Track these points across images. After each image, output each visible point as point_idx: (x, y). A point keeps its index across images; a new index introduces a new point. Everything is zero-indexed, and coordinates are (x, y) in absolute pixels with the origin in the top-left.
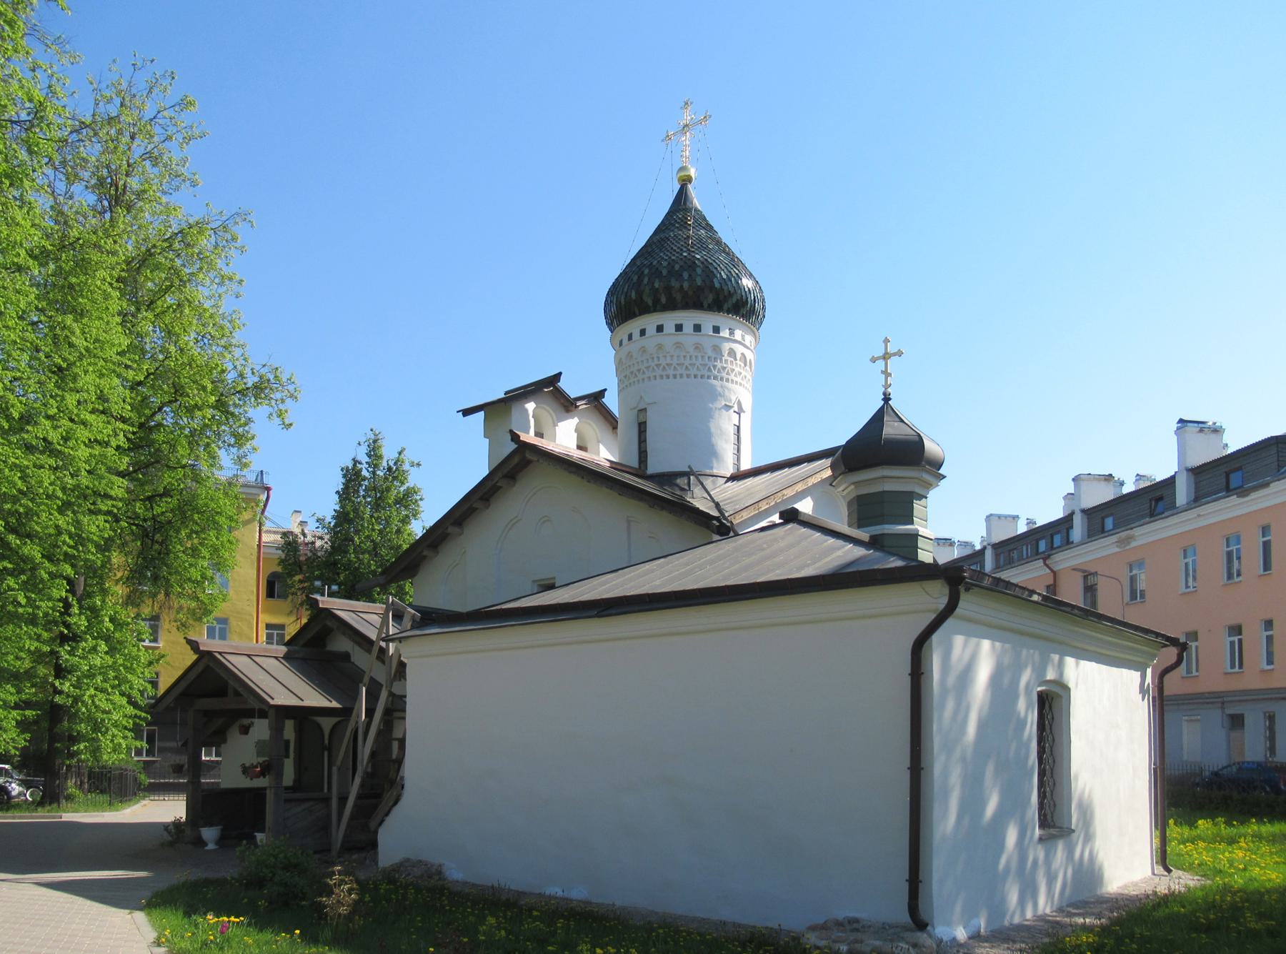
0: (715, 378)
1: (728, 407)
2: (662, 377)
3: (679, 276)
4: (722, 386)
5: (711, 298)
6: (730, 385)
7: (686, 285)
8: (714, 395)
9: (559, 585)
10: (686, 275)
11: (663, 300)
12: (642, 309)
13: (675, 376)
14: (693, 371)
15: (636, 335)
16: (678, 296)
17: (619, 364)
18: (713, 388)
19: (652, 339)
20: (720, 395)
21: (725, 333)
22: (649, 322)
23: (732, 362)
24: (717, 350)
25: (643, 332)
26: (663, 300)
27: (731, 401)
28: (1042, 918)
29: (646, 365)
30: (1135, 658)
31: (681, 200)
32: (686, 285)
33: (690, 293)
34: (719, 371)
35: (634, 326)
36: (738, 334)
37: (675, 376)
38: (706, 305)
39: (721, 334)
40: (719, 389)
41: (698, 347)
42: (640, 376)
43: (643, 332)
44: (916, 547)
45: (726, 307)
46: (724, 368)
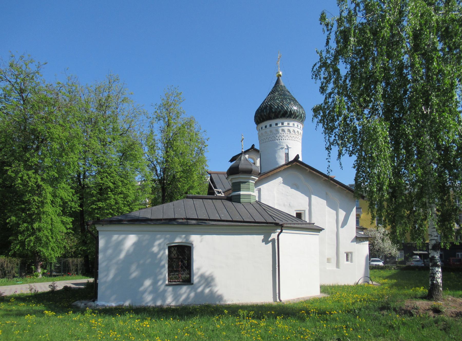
0: (277, 140)
1: (282, 148)
2: (271, 141)
3: (263, 111)
4: (279, 142)
5: (273, 115)
6: (282, 141)
7: (265, 114)
8: (277, 145)
9: (206, 204)
10: (265, 111)
11: (261, 119)
12: (264, 120)
13: (269, 141)
14: (270, 139)
15: (264, 128)
16: (264, 117)
17: (259, 137)
18: (276, 143)
19: (269, 128)
20: (279, 145)
21: (280, 125)
22: (267, 123)
23: (283, 133)
24: (277, 131)
25: (266, 127)
26: (261, 119)
27: (283, 146)
28: (73, 222)
29: (269, 136)
30: (263, 231)
31: (278, 82)
32: (265, 114)
33: (267, 116)
34: (278, 137)
35: (263, 125)
36: (286, 124)
37: (269, 141)
38: (272, 118)
39: (278, 125)
40: (278, 143)
41: (271, 131)
42: (265, 141)
43: (266, 127)
44: (240, 198)
45: (279, 116)
46: (280, 136)
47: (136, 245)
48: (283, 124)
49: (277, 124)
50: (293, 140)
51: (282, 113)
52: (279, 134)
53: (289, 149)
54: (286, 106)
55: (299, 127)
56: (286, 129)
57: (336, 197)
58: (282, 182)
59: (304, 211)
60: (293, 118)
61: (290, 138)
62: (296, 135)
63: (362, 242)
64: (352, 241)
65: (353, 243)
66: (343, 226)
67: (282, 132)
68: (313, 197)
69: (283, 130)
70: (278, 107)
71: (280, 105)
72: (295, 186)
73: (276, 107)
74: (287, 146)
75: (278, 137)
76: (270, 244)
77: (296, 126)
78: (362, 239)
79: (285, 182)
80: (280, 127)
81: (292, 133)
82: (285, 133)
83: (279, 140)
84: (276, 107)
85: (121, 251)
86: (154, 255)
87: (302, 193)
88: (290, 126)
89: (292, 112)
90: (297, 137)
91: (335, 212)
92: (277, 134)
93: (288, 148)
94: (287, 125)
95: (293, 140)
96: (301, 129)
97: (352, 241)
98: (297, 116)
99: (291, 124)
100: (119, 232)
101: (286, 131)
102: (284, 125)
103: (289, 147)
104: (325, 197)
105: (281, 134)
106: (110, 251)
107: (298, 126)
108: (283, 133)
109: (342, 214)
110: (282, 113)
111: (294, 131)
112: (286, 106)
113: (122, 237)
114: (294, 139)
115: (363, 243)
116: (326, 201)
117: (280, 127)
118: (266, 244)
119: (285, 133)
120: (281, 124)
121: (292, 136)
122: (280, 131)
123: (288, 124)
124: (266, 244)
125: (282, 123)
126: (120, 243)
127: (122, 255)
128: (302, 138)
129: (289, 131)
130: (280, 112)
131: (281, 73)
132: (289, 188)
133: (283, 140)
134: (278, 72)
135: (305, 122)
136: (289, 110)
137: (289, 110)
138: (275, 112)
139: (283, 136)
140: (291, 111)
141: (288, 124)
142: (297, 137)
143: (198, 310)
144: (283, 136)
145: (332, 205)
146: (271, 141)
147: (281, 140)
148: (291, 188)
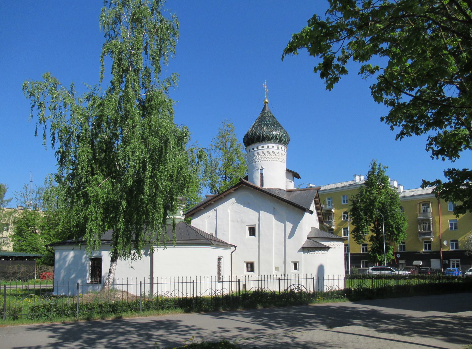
1: (258, 169)
2: (262, 161)
4: (255, 164)
21: (256, 149)
36: (260, 147)
39: (254, 150)
40: (255, 165)
45: (255, 141)
46: (256, 159)
47: (75, 257)
48: (257, 148)
49: (253, 149)
51: (255, 139)
54: (259, 132)
55: (283, 149)
56: (260, 152)
57: (282, 210)
58: (235, 201)
59: (255, 225)
60: (268, 141)
62: (271, 155)
63: (311, 251)
64: (299, 251)
65: (299, 253)
66: (290, 237)
67: (257, 155)
68: (261, 212)
69: (258, 153)
70: (252, 134)
71: (254, 132)
72: (247, 204)
73: (251, 134)
74: (262, 167)
76: (149, 257)
78: (310, 249)
79: (238, 202)
80: (256, 150)
84: (251, 134)
85: (66, 262)
86: (83, 264)
87: (253, 209)
89: (265, 136)
91: (283, 224)
93: (263, 169)
94: (261, 148)
97: (299, 251)
98: (271, 139)
99: (265, 146)
100: (66, 250)
101: (261, 154)
104: (274, 212)
106: (61, 262)
107: (278, 148)
109: (289, 226)
110: (255, 139)
111: (278, 153)
112: (259, 132)
113: (67, 253)
114: (269, 159)
115: (312, 253)
116: (273, 216)
118: (146, 256)
121: (266, 157)
122: (256, 154)
123: (263, 147)
124: (146, 256)
126: (67, 256)
127: (67, 265)
129: (263, 153)
130: (254, 137)
131: (267, 101)
132: (242, 206)
134: (265, 100)
136: (261, 135)
137: (261, 135)
138: (251, 139)
139: (258, 158)
140: (263, 136)
141: (263, 147)
143: (228, 309)
144: (258, 158)
145: (280, 219)
146: (262, 161)
148: (244, 206)
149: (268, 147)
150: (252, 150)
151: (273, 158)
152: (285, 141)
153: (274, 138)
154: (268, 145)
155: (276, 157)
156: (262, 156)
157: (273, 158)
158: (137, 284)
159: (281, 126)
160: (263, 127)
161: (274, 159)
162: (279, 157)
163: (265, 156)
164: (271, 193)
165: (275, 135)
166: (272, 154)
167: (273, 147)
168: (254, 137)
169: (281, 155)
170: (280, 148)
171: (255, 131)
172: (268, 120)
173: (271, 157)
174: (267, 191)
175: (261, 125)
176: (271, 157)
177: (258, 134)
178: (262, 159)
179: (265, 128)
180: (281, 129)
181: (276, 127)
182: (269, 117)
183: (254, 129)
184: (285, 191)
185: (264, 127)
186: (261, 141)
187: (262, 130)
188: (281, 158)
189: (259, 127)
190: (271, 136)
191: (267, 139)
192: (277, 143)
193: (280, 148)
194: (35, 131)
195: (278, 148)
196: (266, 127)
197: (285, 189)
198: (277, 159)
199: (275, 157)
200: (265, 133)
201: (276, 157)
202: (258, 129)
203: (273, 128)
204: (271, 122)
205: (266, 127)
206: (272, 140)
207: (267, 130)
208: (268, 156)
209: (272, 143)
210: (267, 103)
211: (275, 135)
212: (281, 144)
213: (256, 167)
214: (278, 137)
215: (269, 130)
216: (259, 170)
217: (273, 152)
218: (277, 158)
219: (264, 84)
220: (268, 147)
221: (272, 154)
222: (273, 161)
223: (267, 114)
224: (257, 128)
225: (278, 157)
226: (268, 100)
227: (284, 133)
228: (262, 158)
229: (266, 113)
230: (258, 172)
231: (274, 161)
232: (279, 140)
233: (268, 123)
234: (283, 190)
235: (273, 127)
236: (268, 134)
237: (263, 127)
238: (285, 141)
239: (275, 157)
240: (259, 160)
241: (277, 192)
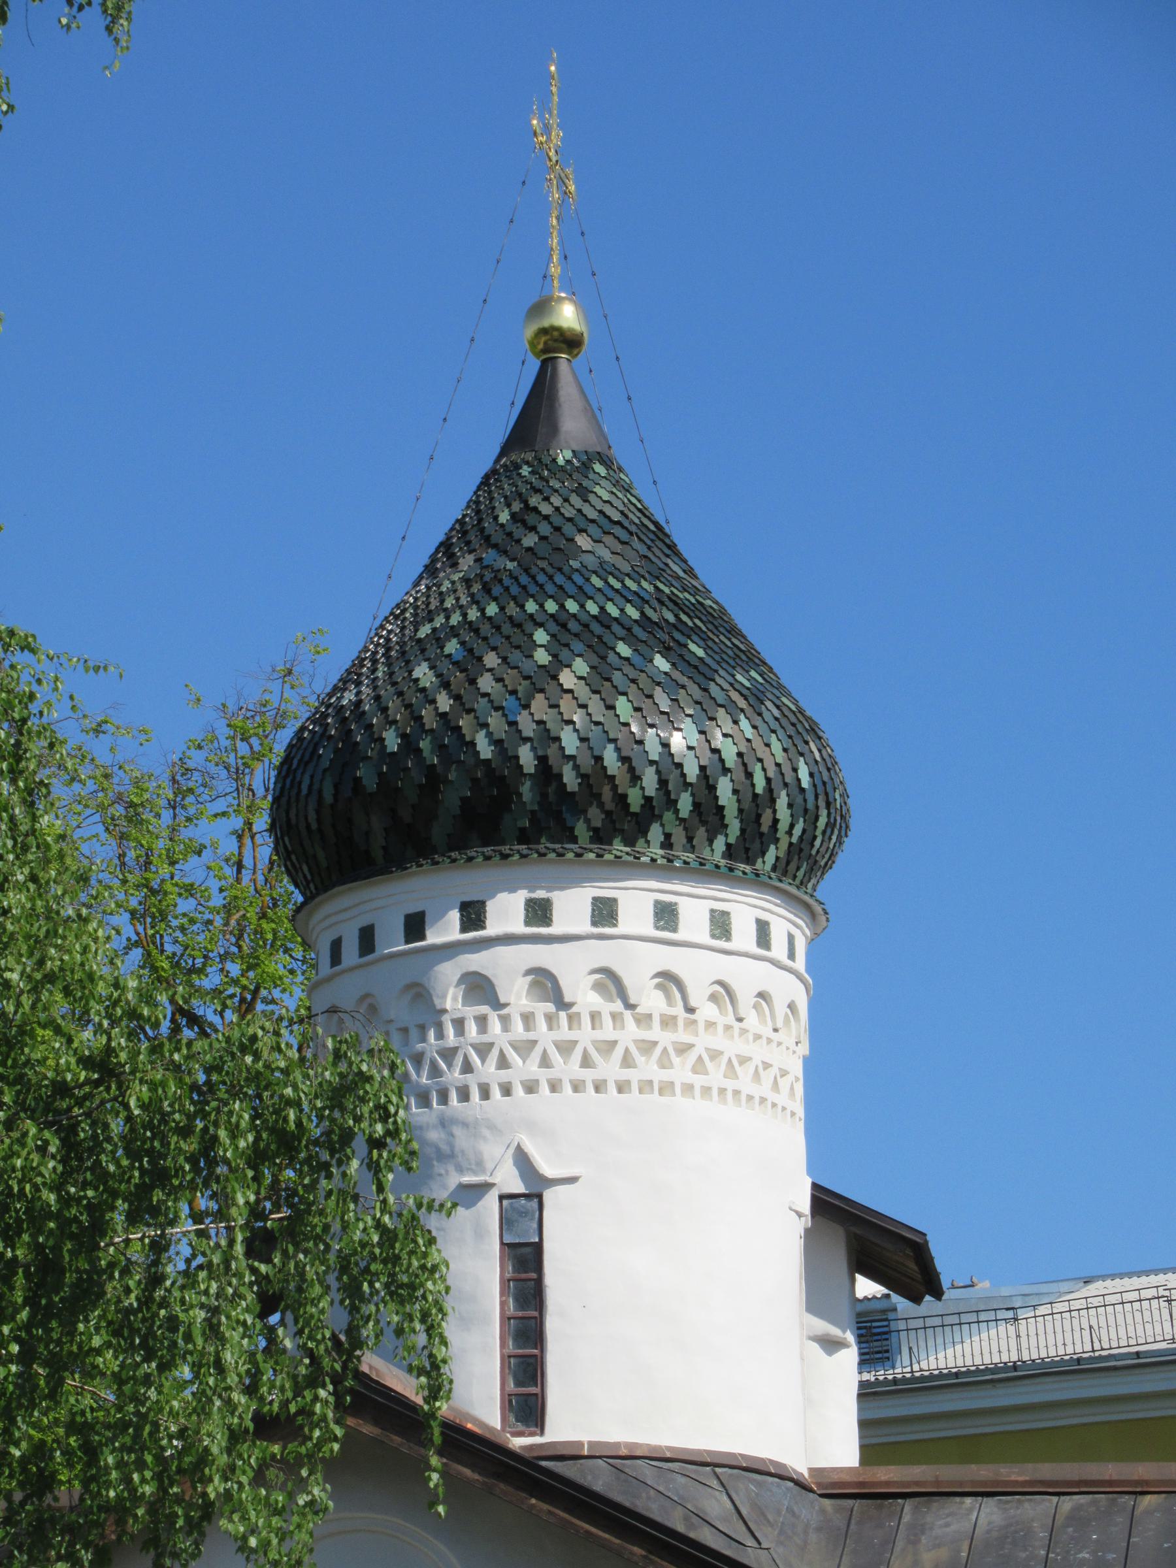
1: (474, 1192)
4: (444, 1123)
23: (482, 1021)
27: (480, 1166)
39: (434, 937)
40: (434, 1135)
45: (438, 833)
46: (448, 1054)
48: (473, 915)
49: (415, 926)
50: (646, 1086)
51: (451, 800)
52: (440, 1035)
53: (549, 1196)
54: (495, 721)
55: (779, 950)
60: (600, 837)
61: (568, 1068)
62: (644, 1020)
67: (471, 1012)
70: (409, 744)
71: (430, 721)
73: (392, 741)
74: (523, 1161)
75: (435, 1072)
77: (702, 934)
80: (451, 950)
81: (707, 1011)
82: (505, 1021)
83: (444, 1098)
84: (392, 741)
88: (554, 930)
89: (570, 779)
90: (665, 1038)
92: (423, 1029)
94: (705, 939)
95: (646, 1086)
96: (800, 964)
98: (650, 812)
102: (493, 928)
103: (548, 1169)
105: (459, 1024)
107: (721, 925)
108: (482, 1021)
110: (451, 800)
111: (725, 992)
112: (495, 721)
114: (609, 1069)
117: (451, 950)
119: (505, 1021)
120: (455, 916)
121: (585, 1035)
122: (452, 1000)
123: (539, 912)
125: (465, 907)
128: (807, 1061)
130: (433, 779)
131: (567, 315)
132: (941, 1277)
133: (485, 1094)
134: (542, 306)
135: (829, 886)
136: (526, 757)
139: (483, 1050)
140: (546, 773)
141: (539, 912)
142: (665, 1038)
147: (464, 1095)
149: (605, 912)
150: (393, 944)
151: (664, 1062)
152: (808, 838)
153: (685, 803)
154: (605, 890)
155: (703, 1041)
156: (528, 1019)
157: (664, 1062)
158: (925, 1328)
159: (749, 658)
160: (542, 657)
161: (681, 1072)
162: (732, 1047)
163: (564, 1032)
164: (654, 1510)
165: (692, 772)
166: (652, 1001)
167: (666, 915)
168: (433, 779)
169: (752, 1020)
170: (744, 935)
171: (444, 703)
172: (604, 570)
173: (647, 1047)
174: (599, 1480)
175: (523, 626)
176: (647, 1047)
177: (485, 750)
178: (524, 1068)
179: (567, 679)
180: (755, 697)
181: (700, 672)
182: (605, 526)
183: (423, 673)
184: (799, 1484)
185: (559, 663)
186: (524, 837)
187: (539, 704)
188: (758, 1052)
189: (491, 660)
190: (650, 780)
191: (596, 816)
192: (703, 872)
193: (744, 935)
194: (252, 856)
195: (721, 925)
196: (581, 666)
197: (800, 1466)
198: (715, 1076)
199: (683, 1049)
200: (570, 742)
201: (703, 1041)
202: (486, 683)
203: (671, 684)
204: (640, 600)
205: (581, 666)
206: (655, 833)
207: (596, 706)
208: (608, 1031)
209: (653, 868)
210: (571, 342)
211: (692, 772)
212: (756, 881)
213: (448, 1156)
214: (724, 790)
215: (623, 706)
216: (490, 1206)
217: (668, 980)
218: (715, 1055)
219: (545, 107)
220: (605, 912)
221: (652, 1001)
222: (666, 1088)
223: (584, 493)
224: (470, 665)
225: (717, 1041)
226: (584, 309)
227: (795, 750)
228: (525, 1048)
229: (565, 471)
230: (480, 1233)
231: (679, 1100)
232: (734, 827)
233: (602, 618)
234: (781, 1475)
235: (661, 663)
236: (610, 757)
237: (542, 657)
238: (808, 838)
239: (683, 1049)
240: (488, 1070)
241: (716, 1505)
